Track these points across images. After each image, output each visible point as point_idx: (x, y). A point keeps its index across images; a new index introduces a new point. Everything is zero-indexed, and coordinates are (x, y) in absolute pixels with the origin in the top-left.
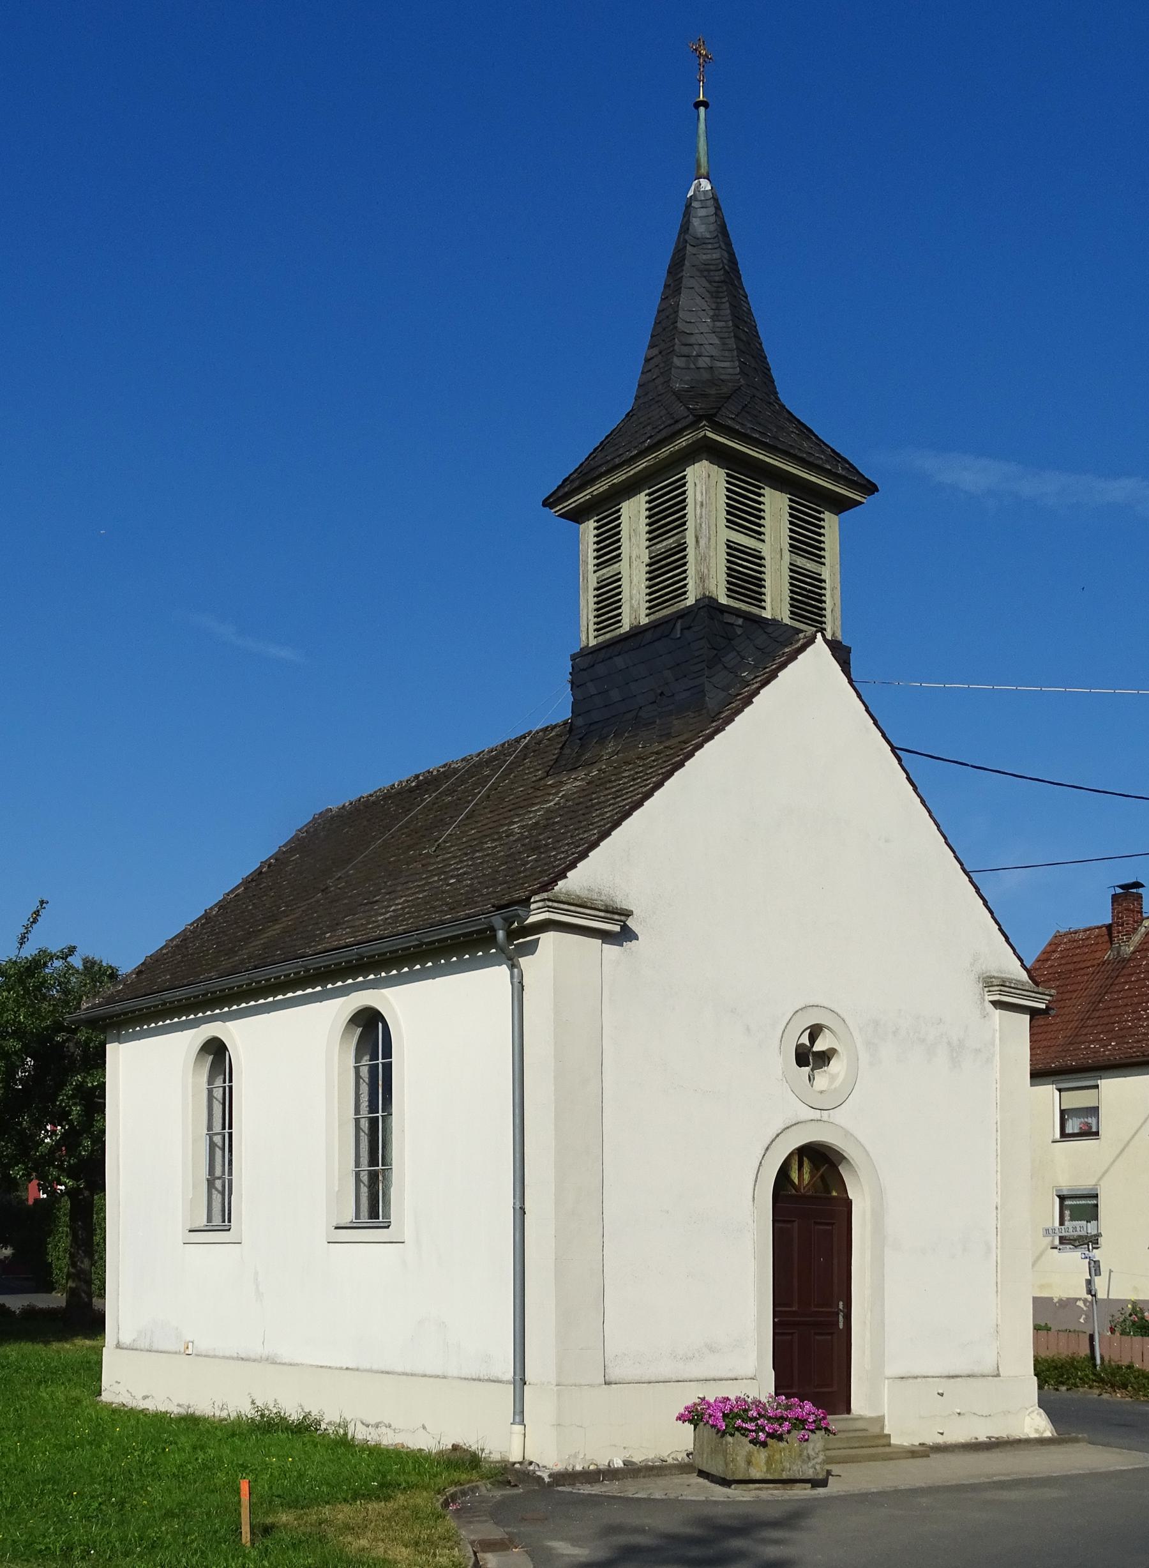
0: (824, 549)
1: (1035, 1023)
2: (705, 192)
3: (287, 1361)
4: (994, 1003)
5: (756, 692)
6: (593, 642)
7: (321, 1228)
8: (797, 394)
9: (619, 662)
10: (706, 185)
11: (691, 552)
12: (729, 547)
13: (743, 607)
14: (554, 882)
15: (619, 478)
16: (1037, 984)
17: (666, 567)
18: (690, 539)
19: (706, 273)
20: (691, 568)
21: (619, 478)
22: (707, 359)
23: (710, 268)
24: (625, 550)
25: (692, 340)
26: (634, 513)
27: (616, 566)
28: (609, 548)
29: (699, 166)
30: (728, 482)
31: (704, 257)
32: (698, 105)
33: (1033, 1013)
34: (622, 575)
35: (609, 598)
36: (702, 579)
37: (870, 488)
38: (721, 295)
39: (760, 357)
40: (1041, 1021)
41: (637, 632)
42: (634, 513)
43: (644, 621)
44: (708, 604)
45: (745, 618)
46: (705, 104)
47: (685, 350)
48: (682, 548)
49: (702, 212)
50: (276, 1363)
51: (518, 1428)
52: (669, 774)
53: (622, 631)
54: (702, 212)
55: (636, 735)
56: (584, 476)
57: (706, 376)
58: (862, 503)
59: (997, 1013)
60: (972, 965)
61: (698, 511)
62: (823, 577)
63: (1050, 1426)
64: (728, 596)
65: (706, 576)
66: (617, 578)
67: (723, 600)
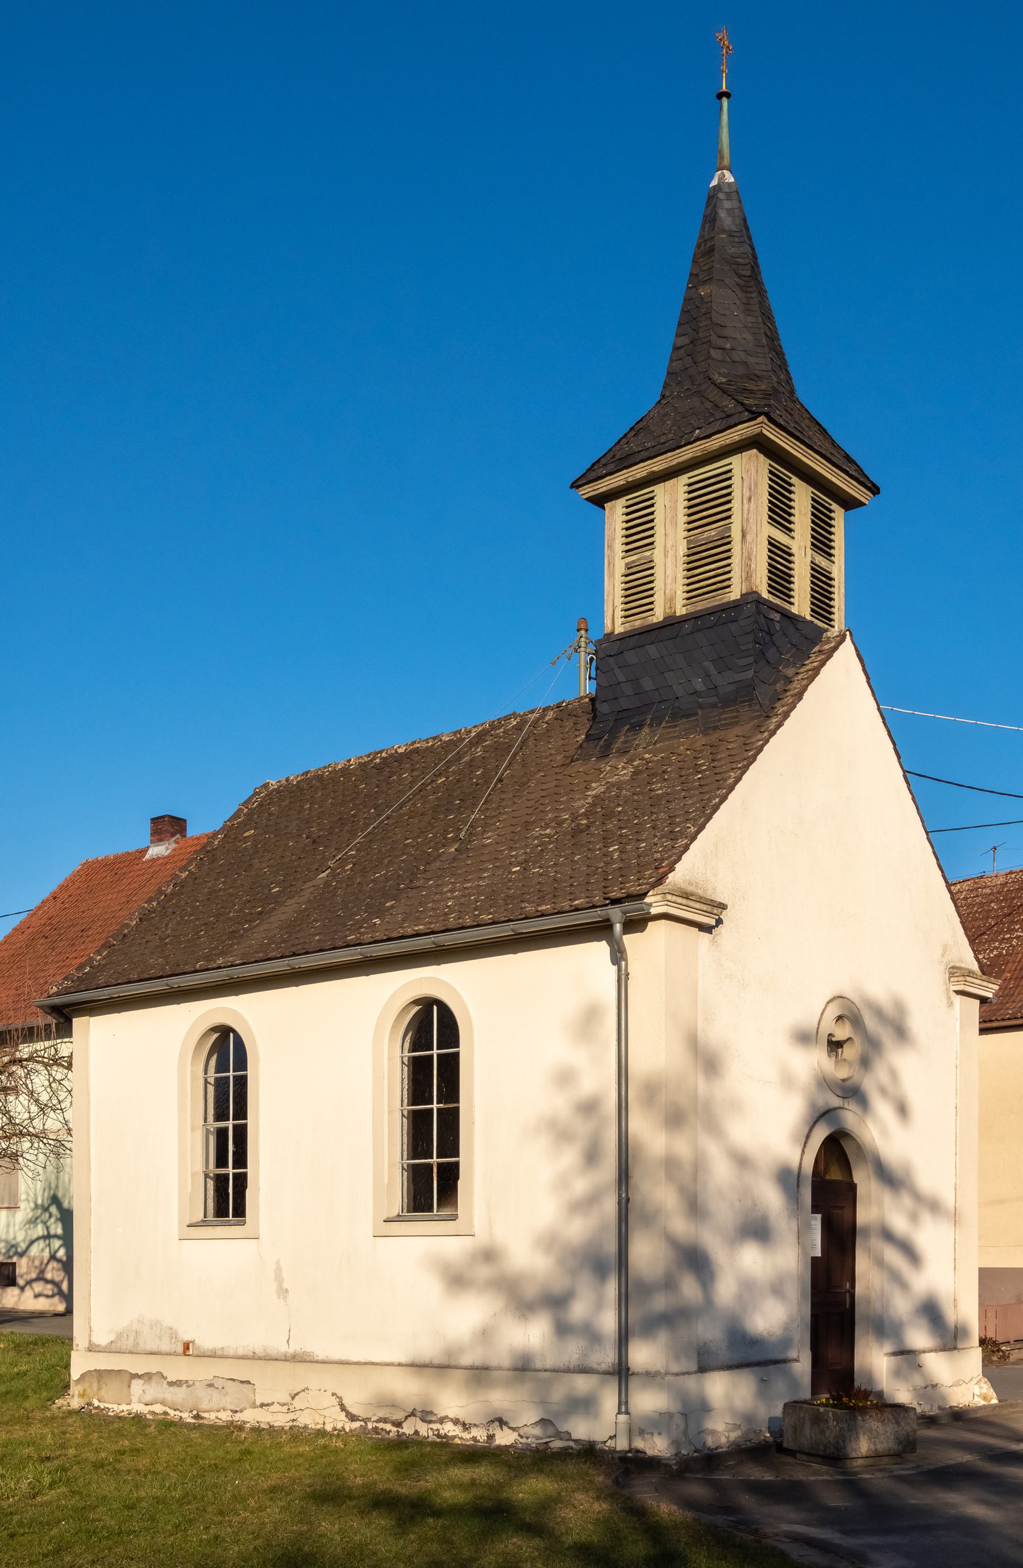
0: (833, 548)
1: (983, 1009)
2: (729, 184)
3: (320, 1358)
4: (958, 992)
5: (805, 689)
6: (619, 629)
7: (366, 1219)
8: (810, 392)
9: (652, 650)
10: (730, 178)
11: (736, 546)
12: (770, 543)
13: (777, 601)
14: (665, 875)
15: (658, 465)
16: (984, 973)
17: (707, 557)
18: (736, 533)
19: (734, 267)
20: (736, 561)
21: (658, 465)
22: (742, 354)
23: (726, 260)
24: (659, 539)
25: (726, 332)
26: (670, 501)
27: (648, 553)
28: (640, 532)
29: (722, 158)
30: (771, 479)
31: (733, 250)
32: (720, 96)
33: (983, 1000)
34: (652, 560)
35: (639, 586)
36: (748, 576)
37: (874, 490)
38: (750, 289)
39: (780, 354)
40: (986, 1007)
41: (671, 623)
42: (670, 501)
43: (681, 611)
44: (751, 598)
45: (783, 614)
46: (727, 95)
47: (720, 342)
48: (725, 540)
49: (727, 204)
50: (305, 1361)
51: (798, 1456)
52: (745, 769)
53: (655, 621)
54: (727, 204)
55: (675, 726)
56: (619, 458)
57: (741, 371)
58: (865, 504)
59: (958, 999)
60: (943, 955)
61: (746, 506)
62: (832, 576)
63: (992, 1393)
64: (769, 592)
65: (747, 573)
66: (649, 566)
67: (765, 595)
